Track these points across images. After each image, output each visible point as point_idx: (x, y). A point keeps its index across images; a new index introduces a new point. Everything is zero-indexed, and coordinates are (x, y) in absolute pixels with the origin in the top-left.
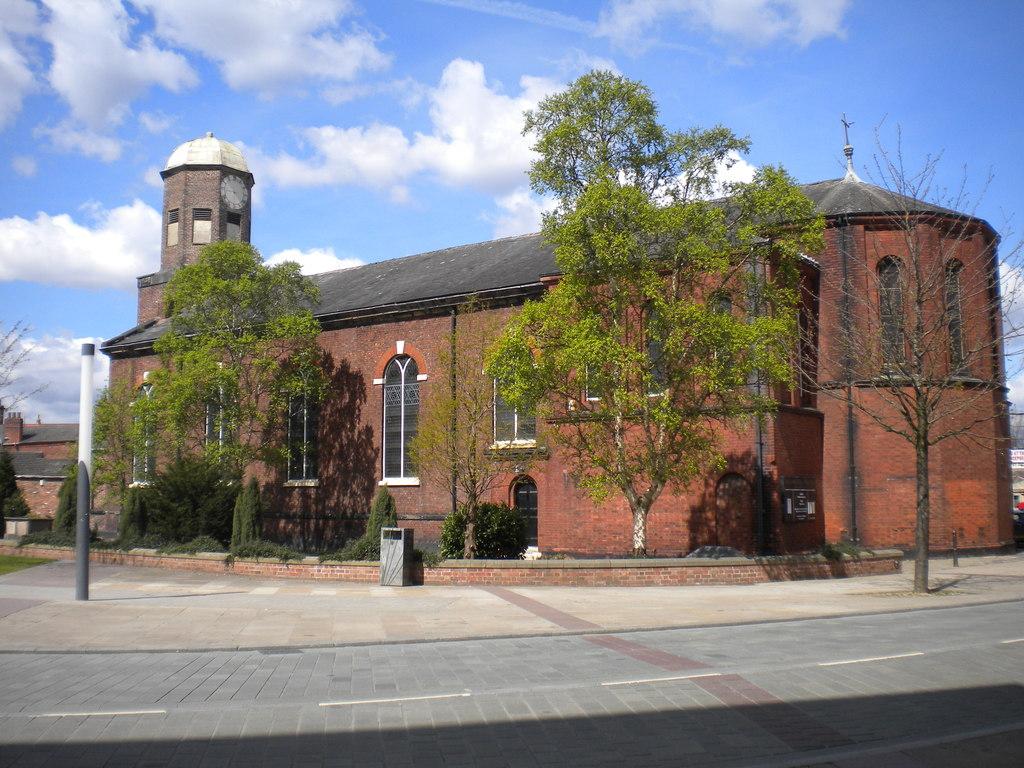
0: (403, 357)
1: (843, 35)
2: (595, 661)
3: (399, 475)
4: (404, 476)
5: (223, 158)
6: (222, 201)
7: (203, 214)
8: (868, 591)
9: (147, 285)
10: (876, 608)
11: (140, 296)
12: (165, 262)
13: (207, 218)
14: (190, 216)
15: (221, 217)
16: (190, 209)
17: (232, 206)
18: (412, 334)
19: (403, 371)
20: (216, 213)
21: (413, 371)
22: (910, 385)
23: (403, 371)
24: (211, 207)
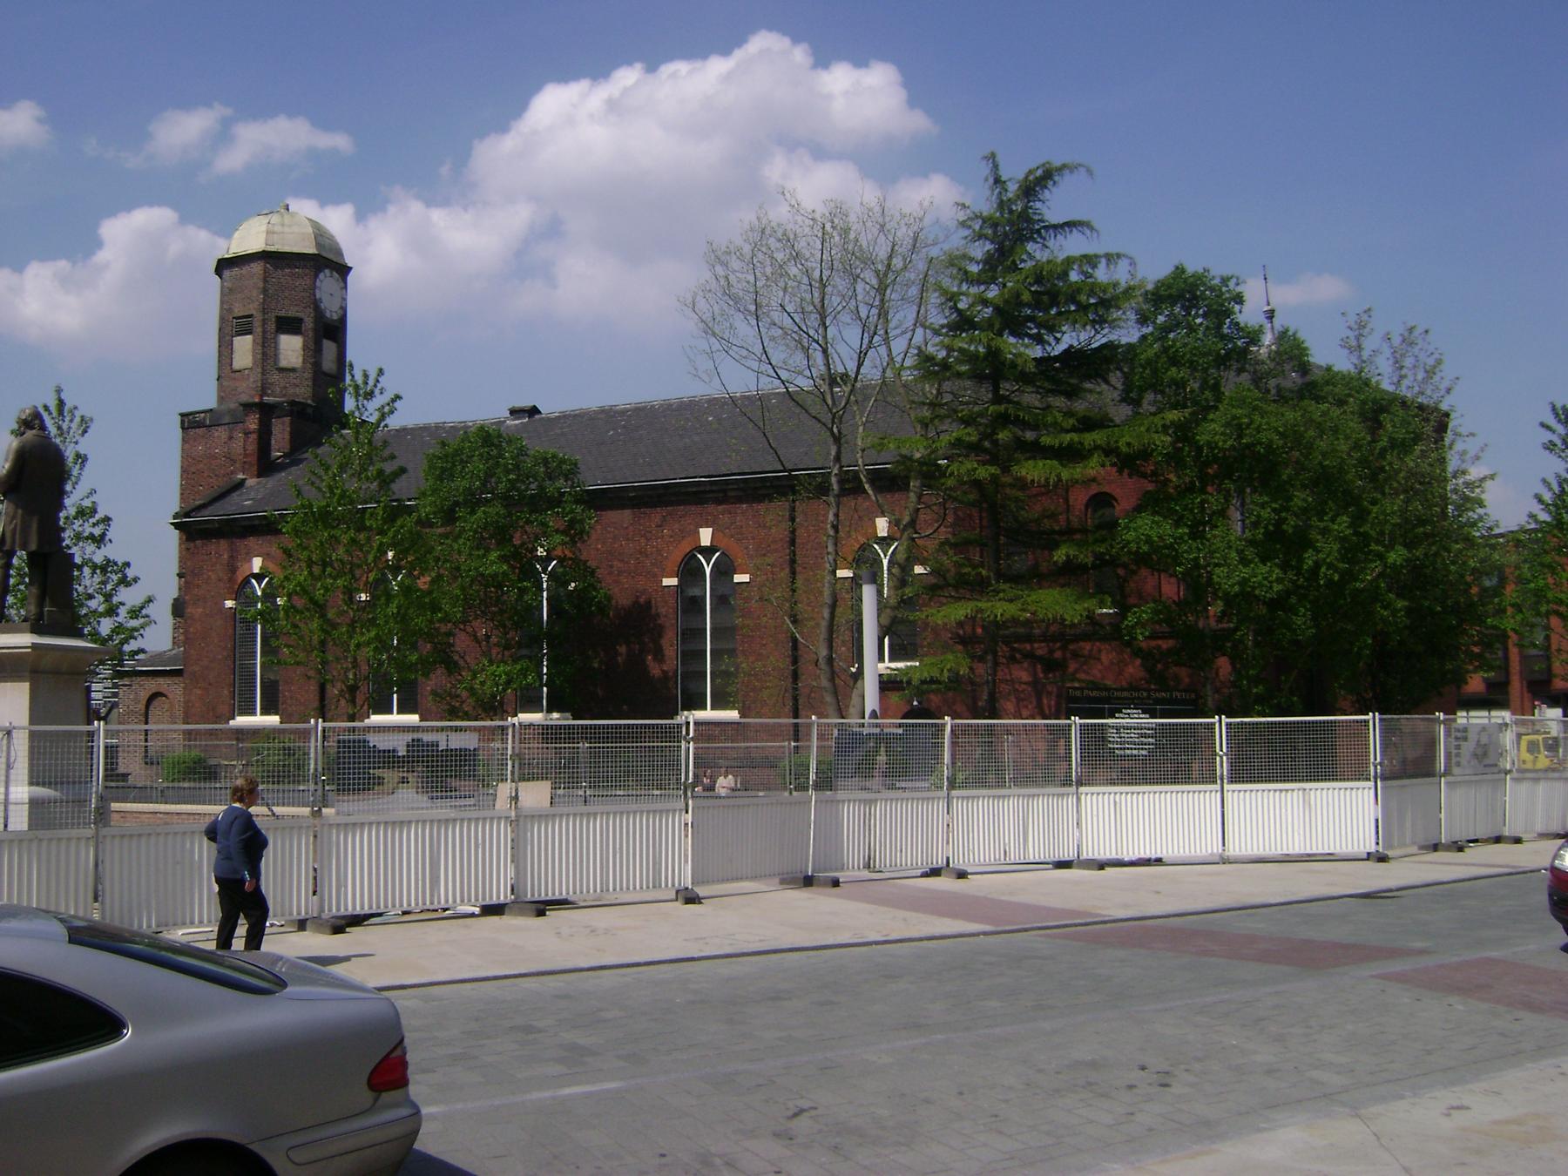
0: (708, 552)
1: (918, 121)
2: (1039, 939)
3: (392, 713)
4: (712, 709)
5: (318, 245)
6: (316, 305)
7: (289, 325)
8: (355, 933)
9: (200, 425)
10: (938, 931)
11: (184, 441)
12: (221, 399)
13: (249, 332)
14: (272, 326)
15: (315, 330)
16: (272, 316)
17: (328, 315)
18: (726, 519)
19: (885, 562)
20: (309, 323)
21: (724, 571)
22: (472, 688)
23: (885, 562)
24: (300, 315)
